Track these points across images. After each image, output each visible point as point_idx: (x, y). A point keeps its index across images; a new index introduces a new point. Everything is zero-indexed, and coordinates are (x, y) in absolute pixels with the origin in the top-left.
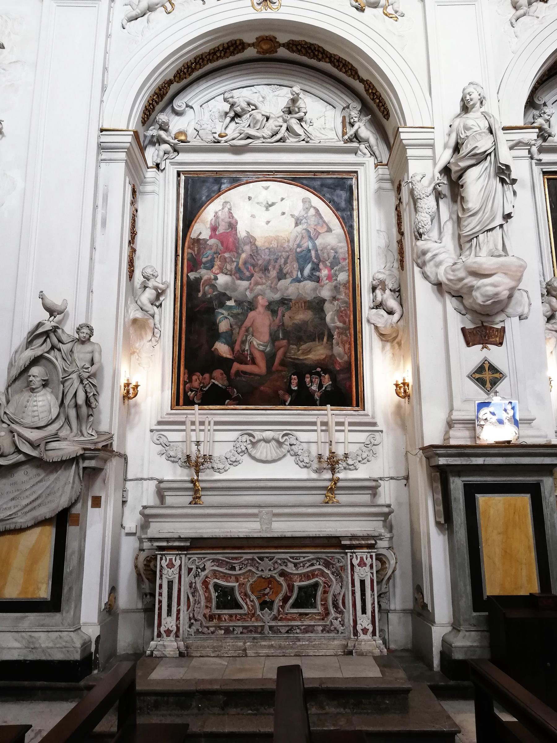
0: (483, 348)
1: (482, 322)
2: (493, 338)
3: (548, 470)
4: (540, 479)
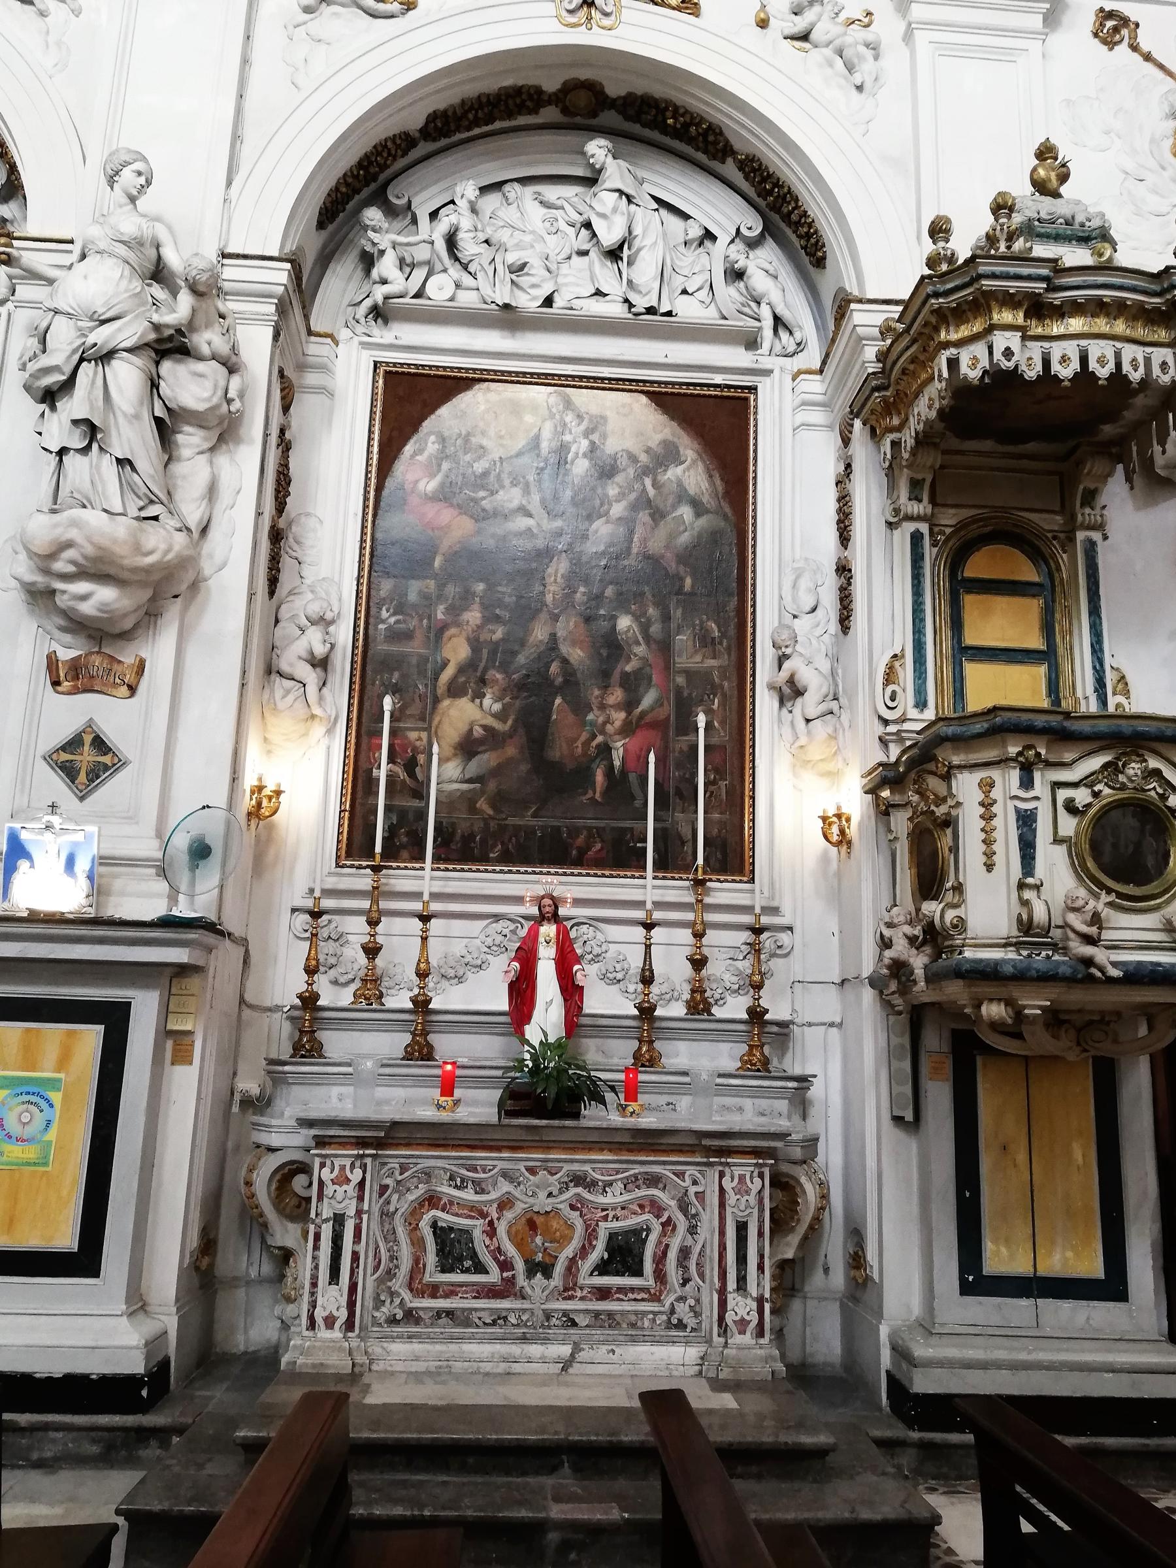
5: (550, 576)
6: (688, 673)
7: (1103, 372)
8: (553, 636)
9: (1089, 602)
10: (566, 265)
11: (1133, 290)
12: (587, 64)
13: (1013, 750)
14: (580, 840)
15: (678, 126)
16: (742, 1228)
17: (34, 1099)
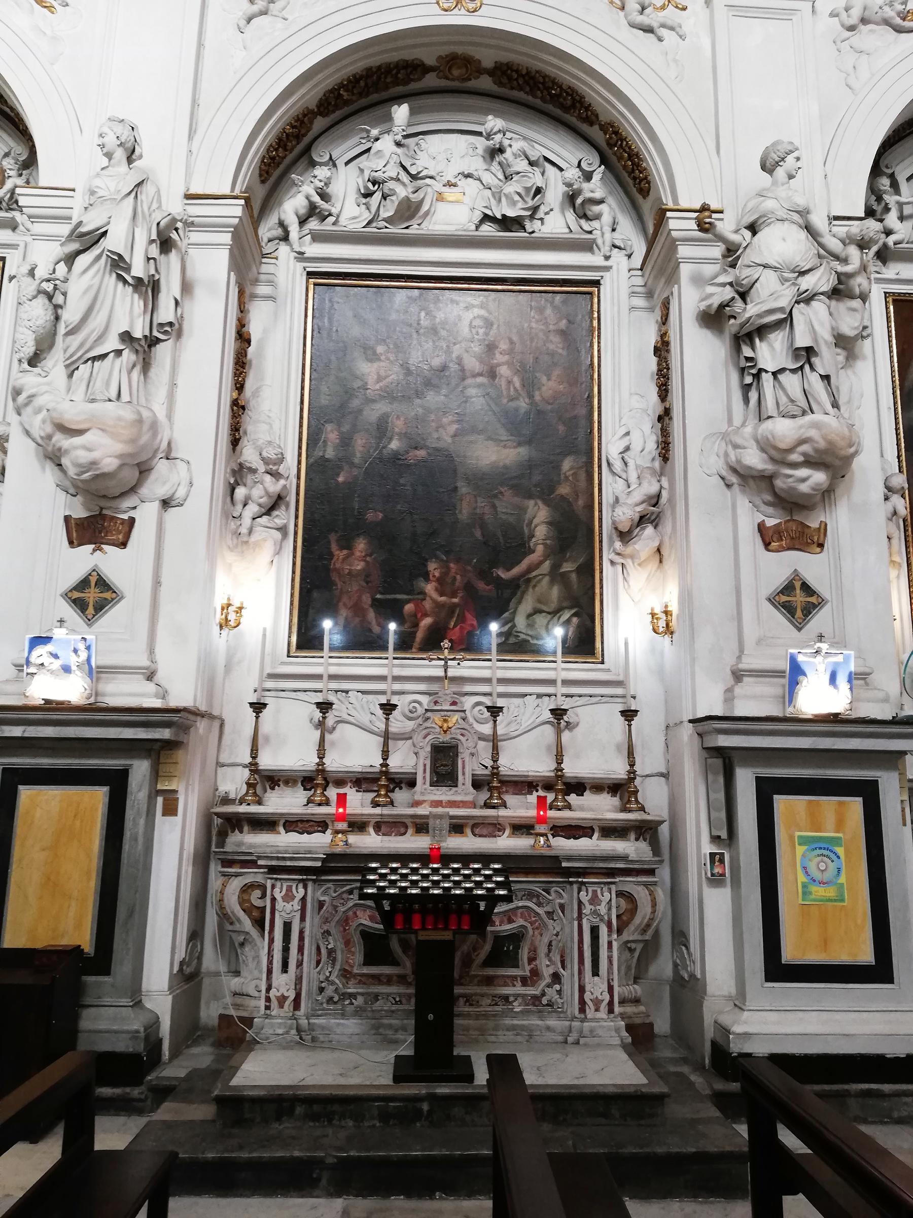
0: (94, 550)
1: (102, 509)
2: (113, 535)
3: (893, 759)
4: (128, 762)
17: (825, 852)
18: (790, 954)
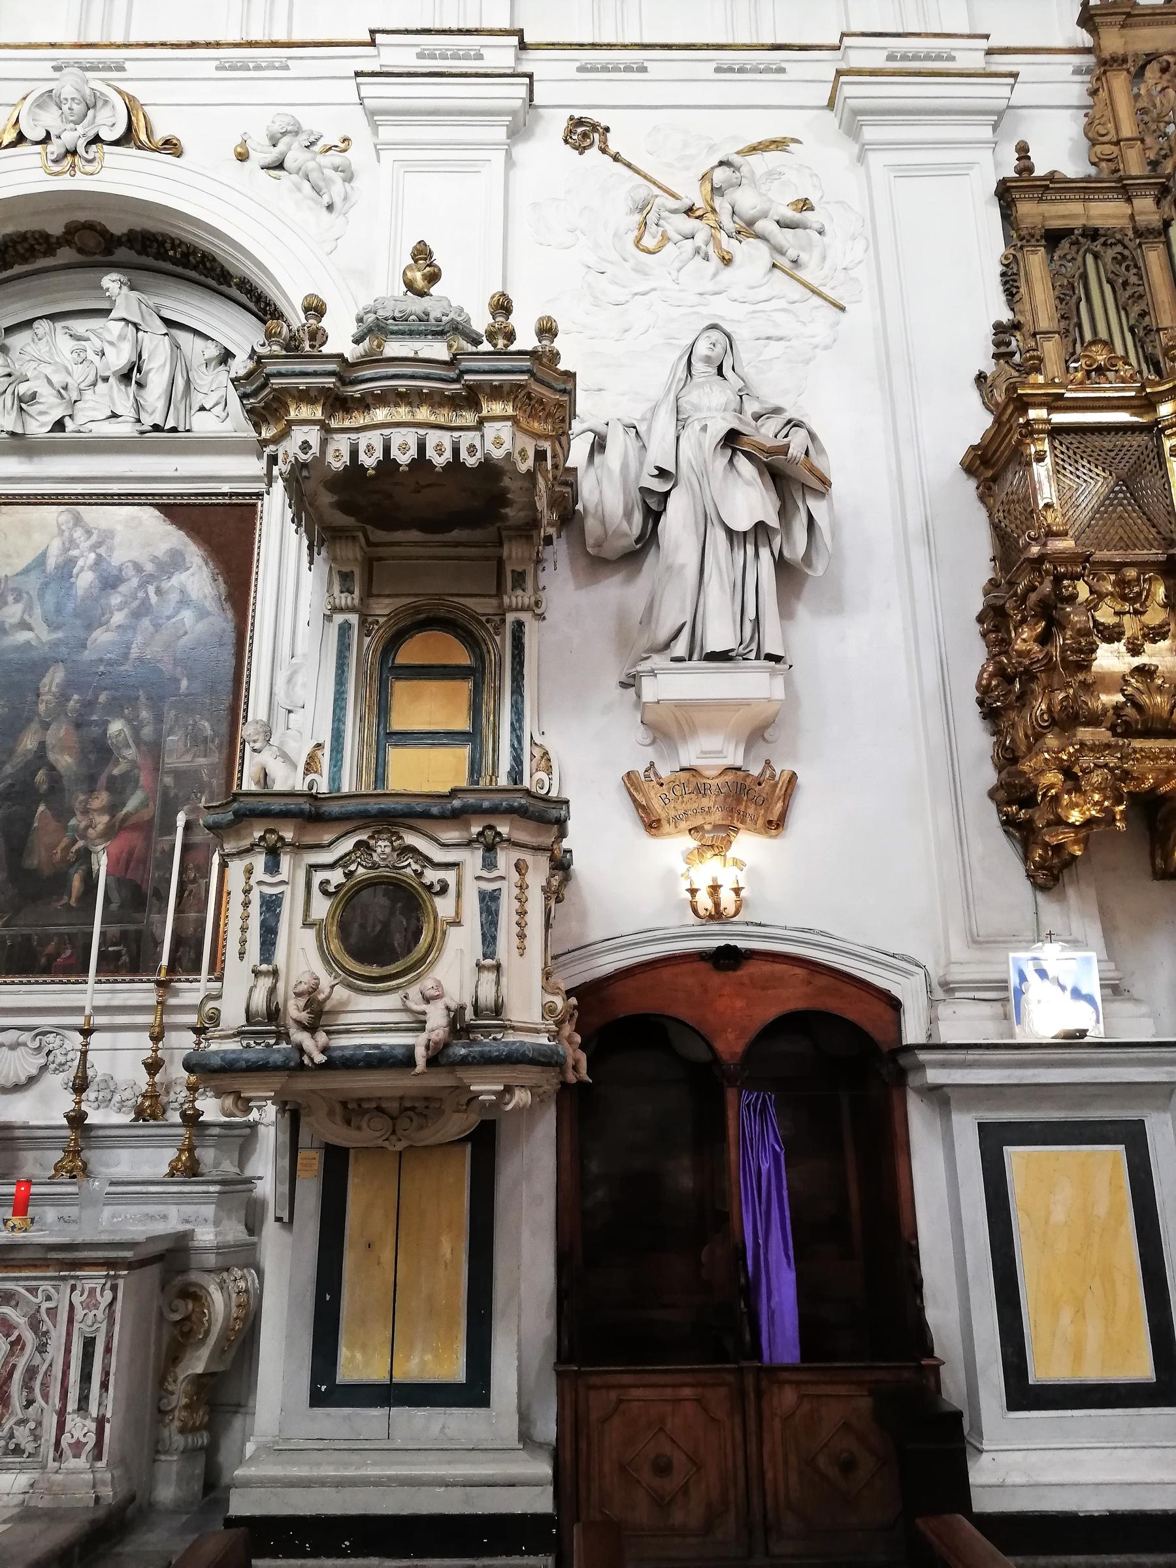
5: (45, 686)
6: (177, 774)
7: (440, 461)
8: (42, 745)
9: (513, 682)
10: (91, 391)
11: (427, 378)
12: (81, 208)
13: (475, 830)
14: (51, 948)
15: (178, 256)
16: (89, 1344)
18: (1039, 1372)
